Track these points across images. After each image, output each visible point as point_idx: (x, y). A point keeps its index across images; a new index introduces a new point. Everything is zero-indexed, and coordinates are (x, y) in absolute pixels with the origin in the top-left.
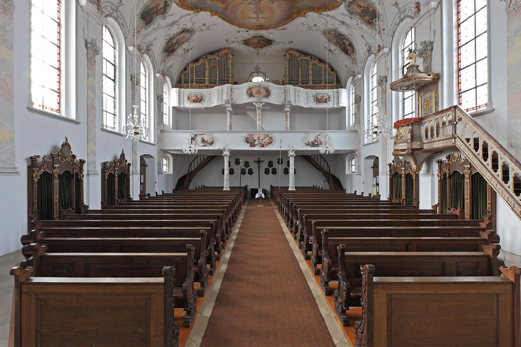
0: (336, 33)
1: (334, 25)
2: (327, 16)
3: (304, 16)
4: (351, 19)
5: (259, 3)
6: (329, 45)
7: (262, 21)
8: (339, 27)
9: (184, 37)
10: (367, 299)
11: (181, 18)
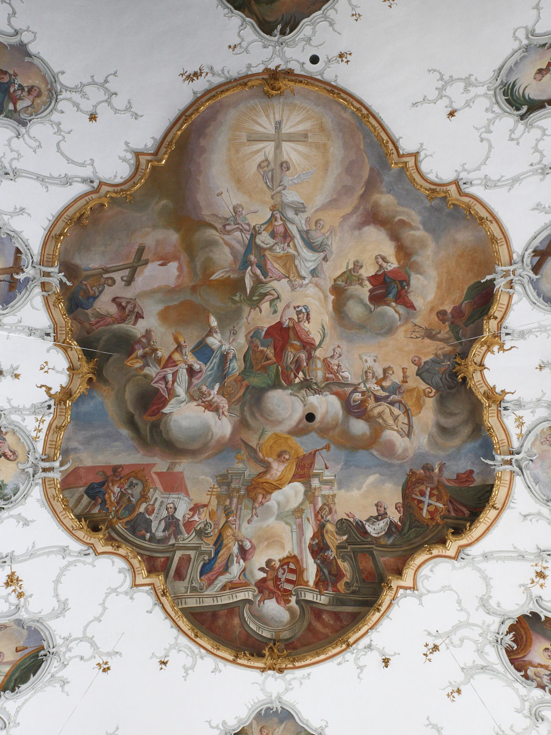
0: (11, 107)
1: (34, 144)
2: (67, 181)
3: (137, 154)
4: (81, 660)
5: (273, 209)
6: (18, 23)
7: (263, 120)
8: (17, 143)
9: (540, 71)
10: (200, 361)
11: (516, 180)
